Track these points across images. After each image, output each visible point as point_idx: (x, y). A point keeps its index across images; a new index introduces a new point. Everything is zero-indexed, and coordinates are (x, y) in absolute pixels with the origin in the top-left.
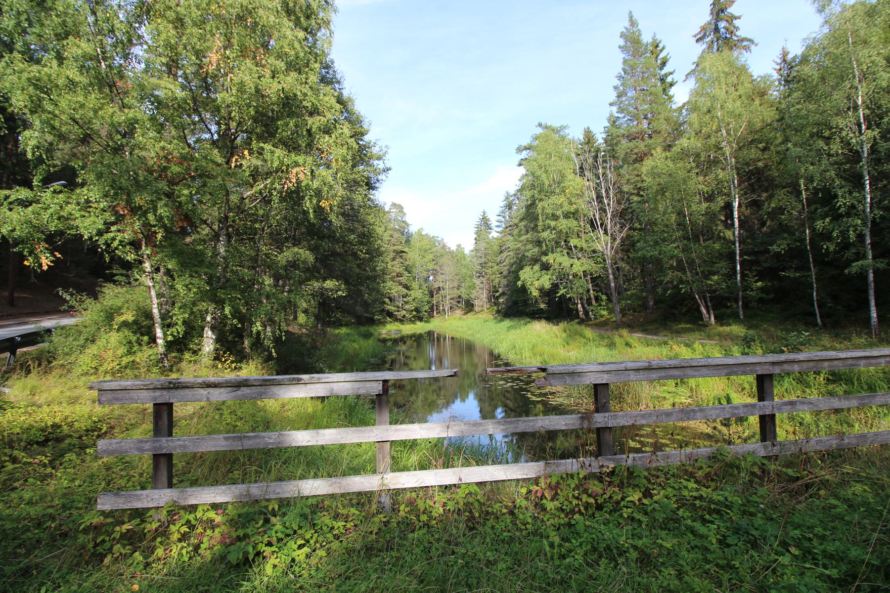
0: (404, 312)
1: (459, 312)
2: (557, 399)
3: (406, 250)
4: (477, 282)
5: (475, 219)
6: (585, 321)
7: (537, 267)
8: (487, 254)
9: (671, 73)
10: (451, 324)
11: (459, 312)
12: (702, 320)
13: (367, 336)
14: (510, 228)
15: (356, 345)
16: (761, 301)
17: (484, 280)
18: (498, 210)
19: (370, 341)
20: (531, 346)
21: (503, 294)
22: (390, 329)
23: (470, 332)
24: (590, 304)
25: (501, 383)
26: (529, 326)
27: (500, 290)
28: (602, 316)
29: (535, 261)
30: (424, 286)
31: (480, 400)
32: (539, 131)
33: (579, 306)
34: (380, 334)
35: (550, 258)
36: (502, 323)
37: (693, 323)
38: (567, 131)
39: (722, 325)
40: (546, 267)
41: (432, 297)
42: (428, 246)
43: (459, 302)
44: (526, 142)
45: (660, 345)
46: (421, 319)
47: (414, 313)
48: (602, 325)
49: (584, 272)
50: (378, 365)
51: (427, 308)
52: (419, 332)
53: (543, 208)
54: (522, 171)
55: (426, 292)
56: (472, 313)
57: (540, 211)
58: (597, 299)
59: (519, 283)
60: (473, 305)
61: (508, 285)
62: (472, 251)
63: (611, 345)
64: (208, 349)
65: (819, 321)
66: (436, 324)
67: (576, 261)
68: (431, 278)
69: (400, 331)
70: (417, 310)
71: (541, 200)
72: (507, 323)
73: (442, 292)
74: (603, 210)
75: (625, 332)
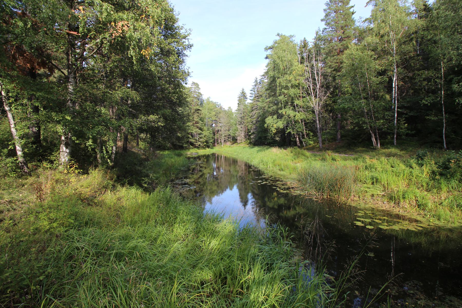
0: (199, 143)
1: (229, 144)
2: (296, 192)
3: (200, 109)
4: (239, 127)
5: (238, 93)
6: (301, 147)
7: (275, 117)
8: (244, 111)
9: (353, 7)
10: (225, 150)
11: (229, 144)
12: (373, 145)
13: (179, 155)
14: (258, 97)
15: (173, 160)
16: (407, 135)
17: (243, 126)
18: (251, 88)
19: (181, 158)
20: (272, 161)
21: (253, 133)
22: (192, 152)
23: (235, 154)
24: (303, 138)
25: (259, 181)
26: (269, 150)
27: (252, 131)
28: (310, 145)
29: (272, 114)
30: (211, 129)
31: (240, 190)
32: (278, 38)
33: (297, 139)
34: (186, 155)
35: (283, 111)
36: (254, 149)
37: (367, 147)
38: (294, 39)
39: (385, 148)
40: (280, 116)
41: (215, 135)
42: (212, 108)
43: (229, 138)
44: (270, 44)
45: (354, 159)
46: (208, 147)
47: (205, 143)
48: (311, 149)
49: (301, 120)
50: (185, 171)
51: (212, 141)
52: (207, 154)
53: (280, 83)
54: (267, 61)
55: (212, 133)
56: (236, 144)
57: (278, 84)
58: (308, 135)
59: (266, 125)
60: (236, 140)
61: (255, 129)
62: (236, 110)
63: (324, 159)
64: (63, 160)
65: (445, 146)
66: (216, 150)
67: (297, 113)
68: (214, 125)
69: (198, 153)
70: (207, 142)
71: (278, 78)
72: (256, 148)
73: (220, 132)
74: (315, 84)
75: (329, 152)
